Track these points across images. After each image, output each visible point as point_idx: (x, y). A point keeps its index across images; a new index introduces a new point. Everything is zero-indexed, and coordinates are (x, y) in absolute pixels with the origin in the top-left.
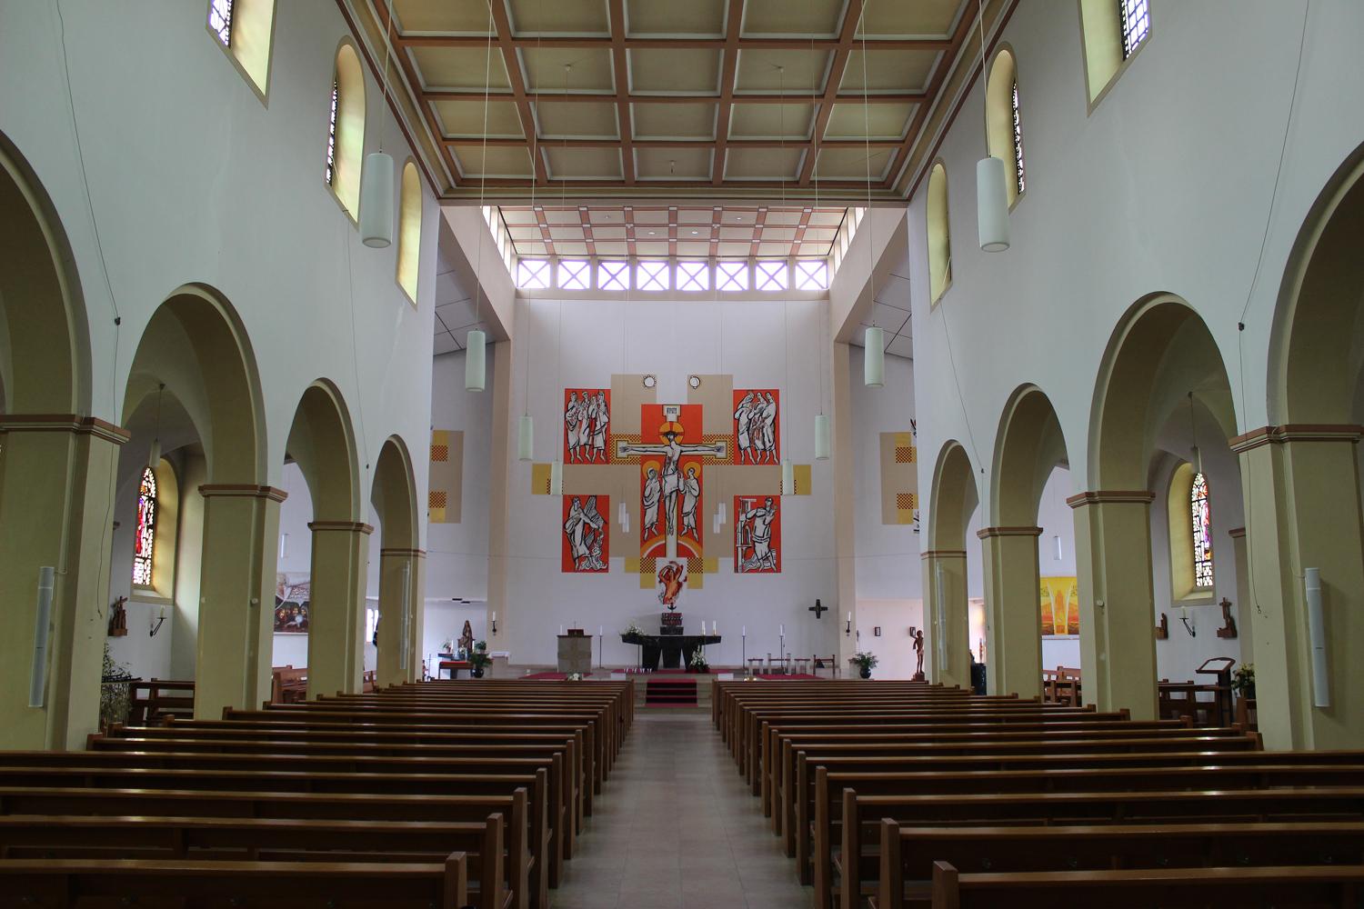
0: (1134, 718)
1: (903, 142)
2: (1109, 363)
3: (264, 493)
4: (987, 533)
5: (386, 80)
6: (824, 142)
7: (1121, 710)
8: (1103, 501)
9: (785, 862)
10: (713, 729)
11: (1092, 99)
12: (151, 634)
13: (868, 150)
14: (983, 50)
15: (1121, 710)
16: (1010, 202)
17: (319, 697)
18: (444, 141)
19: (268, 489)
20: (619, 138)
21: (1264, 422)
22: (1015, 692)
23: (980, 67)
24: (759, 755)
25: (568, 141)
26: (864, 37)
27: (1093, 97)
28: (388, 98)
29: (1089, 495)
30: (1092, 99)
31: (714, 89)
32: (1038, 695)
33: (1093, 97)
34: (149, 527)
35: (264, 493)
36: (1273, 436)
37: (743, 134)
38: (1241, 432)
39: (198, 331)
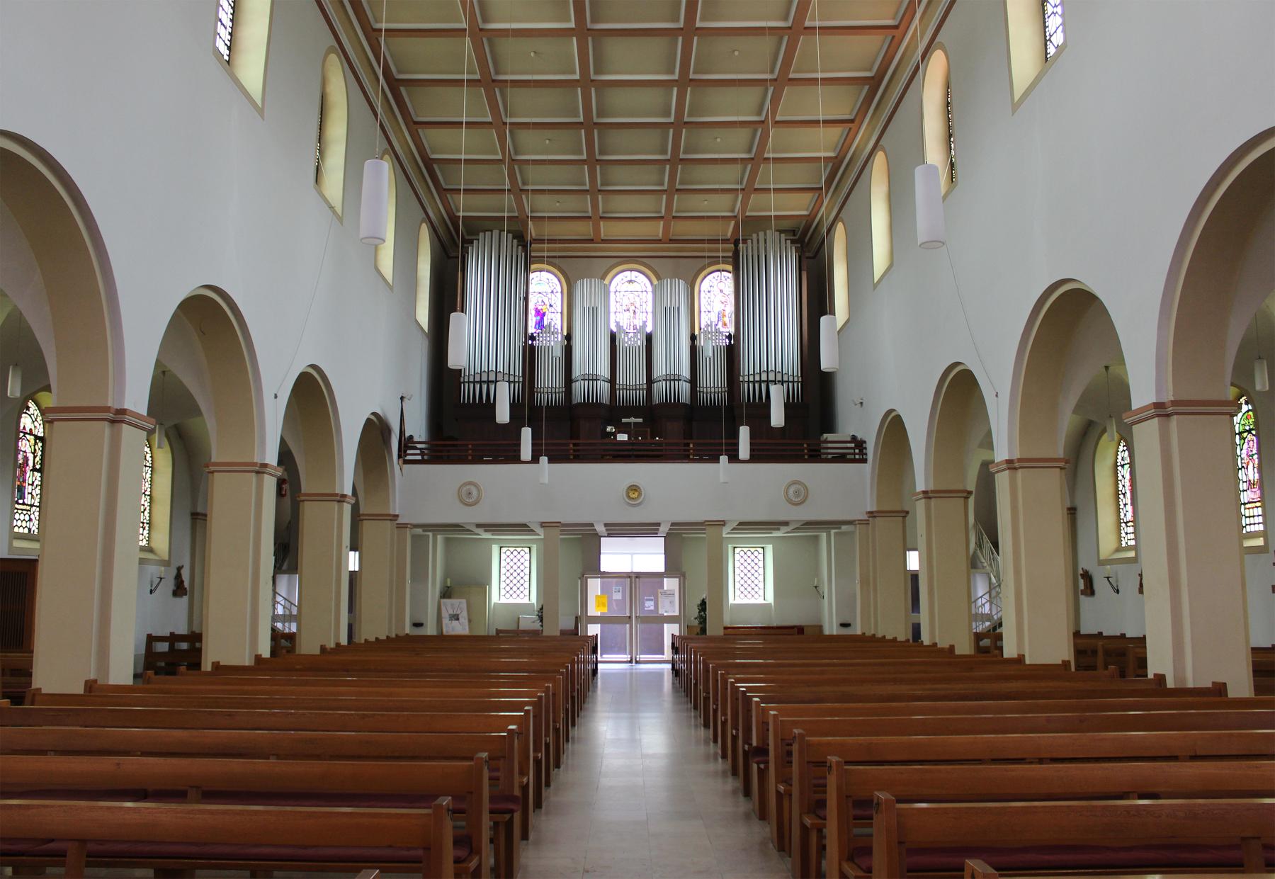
0: (1232, 694)
1: (896, 27)
2: (1027, 343)
3: (119, 417)
4: (1005, 466)
5: (379, 111)
6: (777, 122)
7: (1214, 683)
8: (1177, 413)
9: (720, 765)
10: (707, 758)
11: (1016, 99)
12: (151, 592)
13: (821, 131)
14: (920, 51)
15: (1214, 683)
16: (943, 191)
17: (216, 665)
18: (372, 34)
19: (123, 412)
20: (587, 187)
21: (1151, 398)
22: (1220, 680)
23: (917, 68)
24: (696, 684)
25: (535, 124)
26: (771, 156)
27: (1016, 98)
28: (382, 126)
29: (1158, 405)
30: (1016, 99)
31: (665, 152)
32: (1066, 658)
33: (1016, 98)
34: (34, 470)
35: (119, 417)
36: (1160, 410)
37: (692, 183)
38: (1135, 406)
39: (207, 320)
